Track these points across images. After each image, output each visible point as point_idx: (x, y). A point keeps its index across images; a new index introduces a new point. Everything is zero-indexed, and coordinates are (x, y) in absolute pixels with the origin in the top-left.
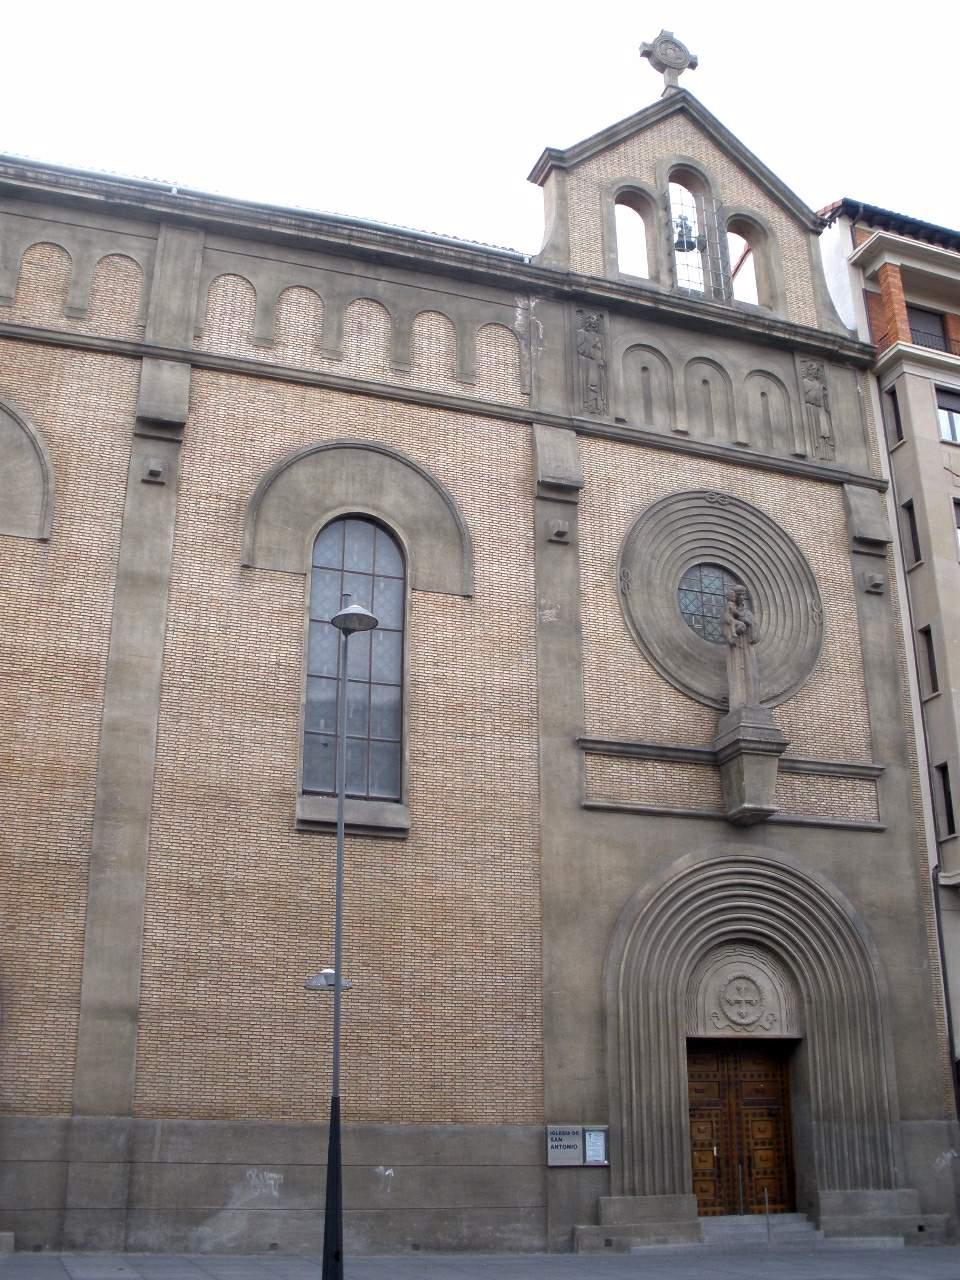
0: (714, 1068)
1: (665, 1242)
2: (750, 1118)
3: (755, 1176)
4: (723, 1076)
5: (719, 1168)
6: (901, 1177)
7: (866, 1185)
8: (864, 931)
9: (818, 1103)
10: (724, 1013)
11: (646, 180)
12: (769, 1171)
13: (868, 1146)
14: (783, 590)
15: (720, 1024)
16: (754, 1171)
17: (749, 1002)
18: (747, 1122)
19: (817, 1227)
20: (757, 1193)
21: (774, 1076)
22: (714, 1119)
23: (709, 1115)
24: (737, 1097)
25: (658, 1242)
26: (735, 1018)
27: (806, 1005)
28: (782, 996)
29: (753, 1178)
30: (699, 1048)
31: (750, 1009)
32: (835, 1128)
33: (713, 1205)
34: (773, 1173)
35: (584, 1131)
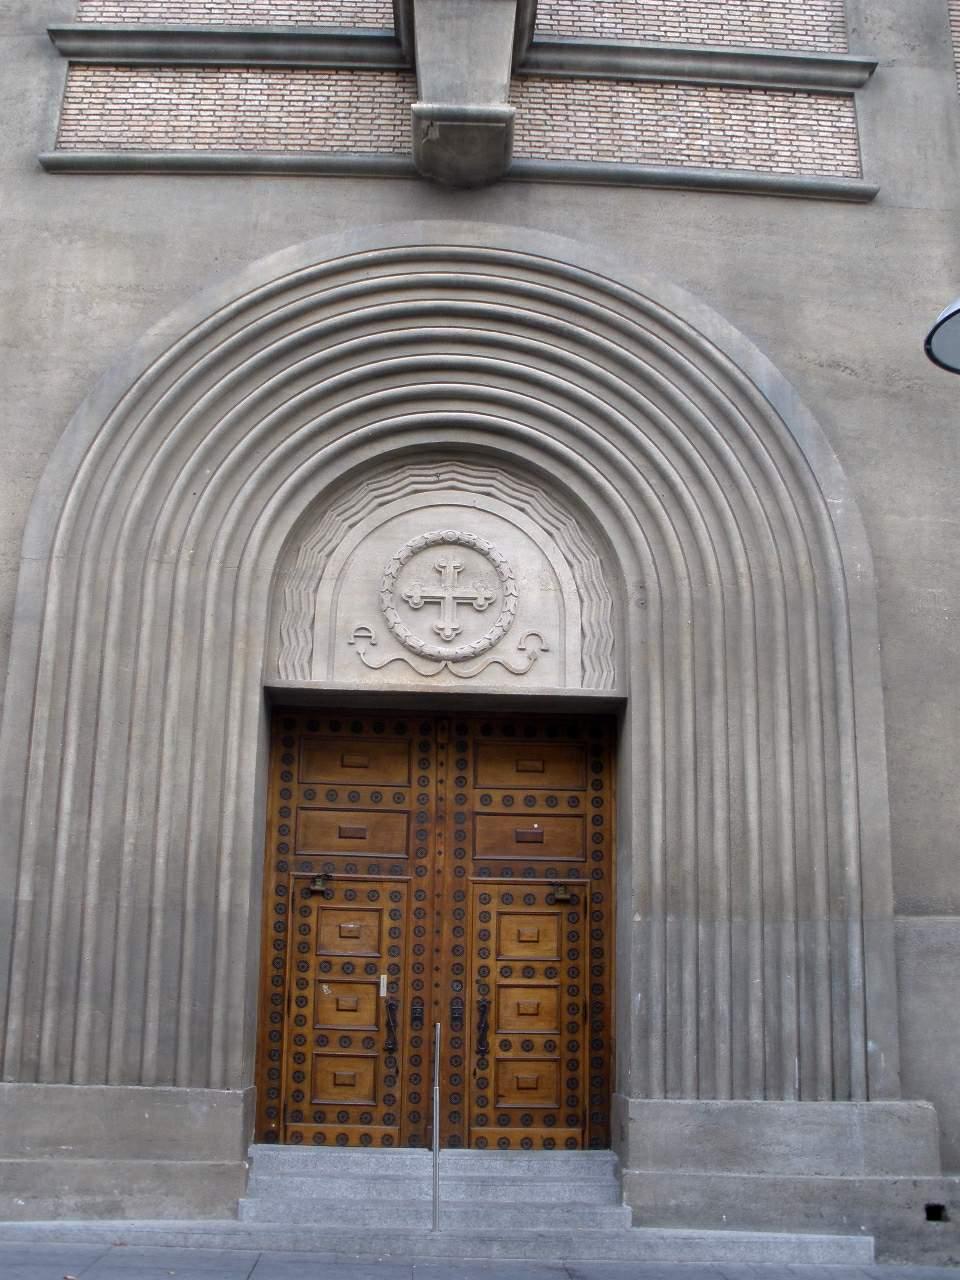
0: (400, 778)
1: (113, 1210)
2: (494, 906)
3: (495, 1052)
4: (423, 799)
5: (391, 1026)
6: (885, 1063)
7: (773, 1087)
8: (804, 421)
9: (649, 863)
10: (391, 630)
12: (539, 1041)
13: (789, 981)
15: (376, 658)
16: (494, 1041)
17: (464, 603)
18: (485, 917)
19: (619, 1187)
20: (498, 1096)
21: (574, 802)
22: (386, 904)
23: (373, 896)
24: (460, 854)
25: (86, 1211)
26: (434, 648)
27: (632, 608)
28: (569, 588)
29: (491, 1058)
30: (302, 724)
31: (468, 619)
32: (694, 932)
33: (366, 1118)
34: (550, 1046)
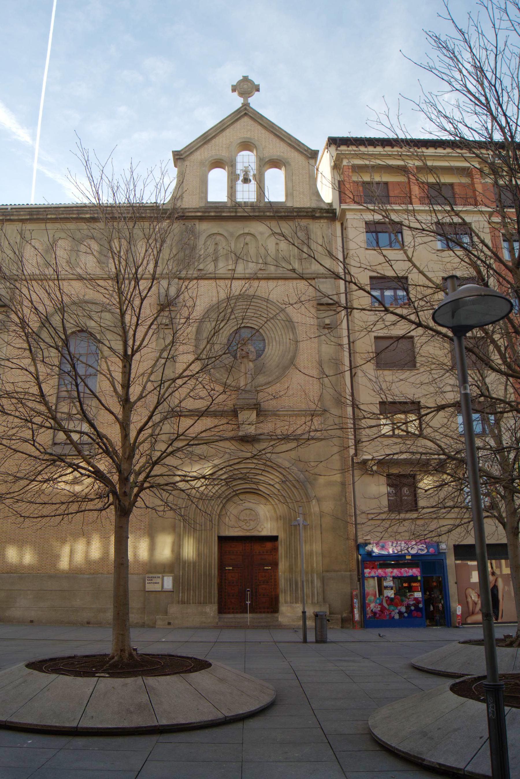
11: (224, 154)
14: (280, 333)
30: (222, 540)
35: (163, 577)
